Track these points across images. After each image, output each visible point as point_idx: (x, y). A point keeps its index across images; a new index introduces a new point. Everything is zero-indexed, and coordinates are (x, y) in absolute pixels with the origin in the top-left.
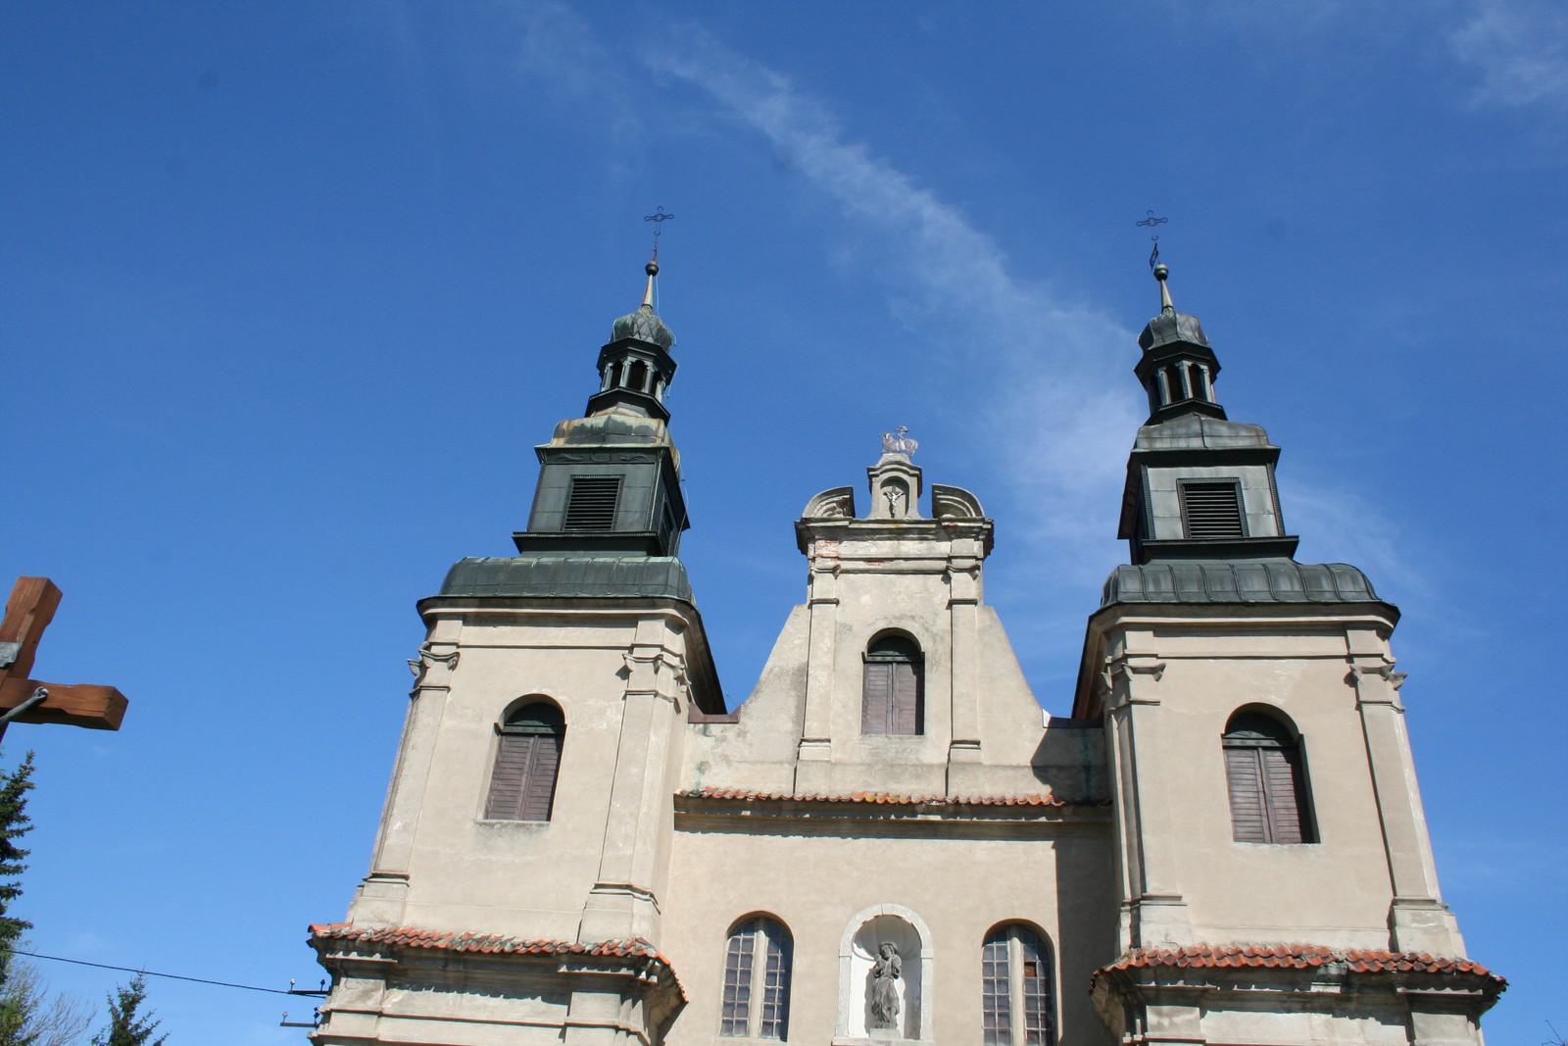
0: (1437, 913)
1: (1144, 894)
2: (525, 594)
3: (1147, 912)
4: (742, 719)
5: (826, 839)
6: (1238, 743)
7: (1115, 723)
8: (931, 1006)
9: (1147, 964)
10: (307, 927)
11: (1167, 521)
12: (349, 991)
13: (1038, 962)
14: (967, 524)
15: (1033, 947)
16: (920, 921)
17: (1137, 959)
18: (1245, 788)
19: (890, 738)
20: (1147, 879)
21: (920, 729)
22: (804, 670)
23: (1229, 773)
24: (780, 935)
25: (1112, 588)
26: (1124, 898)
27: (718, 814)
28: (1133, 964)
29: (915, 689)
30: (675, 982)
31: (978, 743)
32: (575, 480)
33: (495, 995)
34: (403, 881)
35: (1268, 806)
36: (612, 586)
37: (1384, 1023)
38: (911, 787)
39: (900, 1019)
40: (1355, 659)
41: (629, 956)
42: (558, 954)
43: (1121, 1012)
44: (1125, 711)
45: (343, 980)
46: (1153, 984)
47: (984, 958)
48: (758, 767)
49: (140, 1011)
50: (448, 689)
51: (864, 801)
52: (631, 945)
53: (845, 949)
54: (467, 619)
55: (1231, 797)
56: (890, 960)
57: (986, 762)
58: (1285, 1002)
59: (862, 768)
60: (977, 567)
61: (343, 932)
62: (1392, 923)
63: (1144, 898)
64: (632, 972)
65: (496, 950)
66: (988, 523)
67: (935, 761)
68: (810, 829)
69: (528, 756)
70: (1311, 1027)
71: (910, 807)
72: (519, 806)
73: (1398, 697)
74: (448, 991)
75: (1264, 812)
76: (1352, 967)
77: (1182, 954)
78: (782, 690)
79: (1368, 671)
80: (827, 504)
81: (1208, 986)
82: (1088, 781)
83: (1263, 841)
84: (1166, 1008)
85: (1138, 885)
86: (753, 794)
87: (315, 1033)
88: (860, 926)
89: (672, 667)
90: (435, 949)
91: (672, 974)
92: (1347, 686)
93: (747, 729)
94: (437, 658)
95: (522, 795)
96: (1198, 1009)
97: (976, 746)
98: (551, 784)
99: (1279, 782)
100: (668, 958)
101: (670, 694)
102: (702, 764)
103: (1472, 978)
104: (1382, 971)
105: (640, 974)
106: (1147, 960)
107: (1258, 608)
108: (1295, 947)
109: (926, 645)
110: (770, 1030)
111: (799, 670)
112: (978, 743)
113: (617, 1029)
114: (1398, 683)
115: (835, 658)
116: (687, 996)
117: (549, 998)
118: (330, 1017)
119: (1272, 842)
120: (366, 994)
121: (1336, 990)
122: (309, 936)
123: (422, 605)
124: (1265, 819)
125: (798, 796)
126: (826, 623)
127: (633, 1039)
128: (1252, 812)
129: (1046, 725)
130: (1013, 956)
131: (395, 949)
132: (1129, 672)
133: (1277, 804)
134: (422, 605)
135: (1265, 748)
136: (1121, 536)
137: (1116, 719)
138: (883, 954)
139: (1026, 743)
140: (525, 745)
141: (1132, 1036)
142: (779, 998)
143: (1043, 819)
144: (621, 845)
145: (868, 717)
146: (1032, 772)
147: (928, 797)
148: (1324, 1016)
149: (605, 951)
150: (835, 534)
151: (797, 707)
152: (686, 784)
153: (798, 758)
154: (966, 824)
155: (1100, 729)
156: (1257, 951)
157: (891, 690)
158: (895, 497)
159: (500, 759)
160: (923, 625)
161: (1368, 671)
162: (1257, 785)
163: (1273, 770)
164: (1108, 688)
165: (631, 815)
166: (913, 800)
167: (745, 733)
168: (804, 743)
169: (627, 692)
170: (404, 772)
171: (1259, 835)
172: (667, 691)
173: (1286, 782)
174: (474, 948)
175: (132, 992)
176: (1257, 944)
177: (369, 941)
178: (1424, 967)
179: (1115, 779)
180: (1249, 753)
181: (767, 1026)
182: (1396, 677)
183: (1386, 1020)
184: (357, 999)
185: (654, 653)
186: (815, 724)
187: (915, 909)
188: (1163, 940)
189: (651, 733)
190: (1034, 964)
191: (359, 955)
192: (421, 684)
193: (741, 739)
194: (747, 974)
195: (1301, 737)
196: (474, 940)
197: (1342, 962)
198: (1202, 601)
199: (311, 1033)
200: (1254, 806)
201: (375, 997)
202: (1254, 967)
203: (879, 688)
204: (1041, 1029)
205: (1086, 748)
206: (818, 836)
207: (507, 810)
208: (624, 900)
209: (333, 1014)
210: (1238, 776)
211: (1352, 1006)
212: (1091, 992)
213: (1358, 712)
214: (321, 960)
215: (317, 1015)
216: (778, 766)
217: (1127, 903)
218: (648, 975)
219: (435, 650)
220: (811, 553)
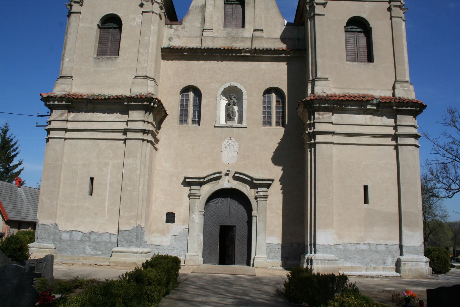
0: (409, 85)
1: (316, 77)
3: (317, 83)
4: (184, 23)
5: (212, 62)
6: (349, 30)
7: (309, 22)
8: (246, 114)
9: (316, 98)
10: (40, 94)
12: (56, 114)
13: (280, 101)
15: (279, 96)
17: (313, 97)
18: (351, 45)
19: (233, 29)
20: (317, 72)
21: (243, 26)
22: (204, 6)
23: (346, 40)
24: (198, 93)
26: (309, 79)
27: (176, 54)
28: (312, 98)
29: (242, 13)
30: (163, 107)
33: (104, 113)
34: (71, 78)
35: (358, 51)
37: (388, 118)
38: (241, 45)
39: (236, 118)
41: (147, 98)
42: (124, 98)
43: (307, 115)
44: (313, 18)
45: (54, 111)
46: (318, 105)
47: (263, 99)
48: (189, 39)
49: (8, 134)
50: (80, 13)
51: (224, 49)
52: (148, 95)
53: (218, 97)
55: (346, 47)
56: (233, 100)
57: (265, 37)
58: (358, 111)
61: (52, 95)
62: (394, 88)
63: (316, 78)
64: (148, 103)
65: (103, 98)
67: (248, 36)
68: (207, 59)
69: (110, 35)
70: (366, 119)
71: (240, 51)
72: (108, 52)
73: (404, 16)
74: (89, 113)
75: (356, 53)
76: (381, 101)
77: (327, 96)
78: (197, 13)
79: (395, 6)
81: (335, 106)
83: (355, 61)
84: (321, 113)
85: (314, 75)
86: (188, 47)
87: (47, 128)
88: (223, 89)
90: (82, 99)
91: (162, 104)
92: (388, 11)
93: (185, 26)
95: (109, 48)
96: (331, 113)
98: (119, 44)
99: (362, 43)
100: (159, 98)
101: (158, 12)
104: (390, 102)
105: (151, 104)
106: (316, 97)
108: (363, 95)
110: (195, 123)
111: (202, 6)
113: (144, 121)
114: (405, 11)
115: (214, 2)
116: (168, 112)
117: (122, 113)
118: (51, 123)
119: (358, 62)
120: (62, 115)
121: (375, 108)
122: (41, 97)
124: (356, 55)
125: (203, 48)
127: (150, 125)
129: (285, 25)
130: (272, 98)
131: (70, 100)
132: (315, 4)
133: (361, 50)
135: (358, 32)
137: (310, 21)
138: (231, 98)
139: (279, 31)
140: (109, 32)
141: (310, 121)
142: (197, 113)
143: (283, 55)
145: (226, 22)
146: (280, 40)
147: (246, 48)
148: (370, 116)
149: (139, 97)
152: (165, 44)
153: (202, 35)
154: (258, 57)
157: (233, 13)
159: (101, 37)
161: (395, 6)
164: (307, 10)
165: (146, 53)
166: (241, 49)
168: (204, 31)
169: (143, 11)
170: (68, 42)
171: (354, 60)
172: (157, 11)
173: (364, 43)
174: (95, 98)
175: (5, 128)
176: (351, 94)
177: (61, 97)
178: (403, 101)
179: (308, 41)
180: (353, 33)
181: (194, 122)
182: (404, 9)
183: (388, 117)
184: (59, 116)
186: (208, 24)
187: (241, 84)
188: (322, 91)
189: (152, 26)
190: (279, 101)
191: (58, 102)
192: (71, 11)
193: (183, 30)
194: (187, 105)
195: (371, 28)
196: (95, 95)
197: (378, 99)
199: (45, 128)
200: (353, 50)
201: (65, 115)
202: (350, 100)
203: (230, 12)
204: (280, 121)
206: (209, 61)
207: (104, 54)
208: (145, 81)
209: (52, 121)
210: (349, 41)
211: (379, 113)
212: (297, 109)
213: (390, 20)
214: (46, 105)
215: (47, 123)
216: (196, 38)
217: (311, 80)
218: (154, 104)
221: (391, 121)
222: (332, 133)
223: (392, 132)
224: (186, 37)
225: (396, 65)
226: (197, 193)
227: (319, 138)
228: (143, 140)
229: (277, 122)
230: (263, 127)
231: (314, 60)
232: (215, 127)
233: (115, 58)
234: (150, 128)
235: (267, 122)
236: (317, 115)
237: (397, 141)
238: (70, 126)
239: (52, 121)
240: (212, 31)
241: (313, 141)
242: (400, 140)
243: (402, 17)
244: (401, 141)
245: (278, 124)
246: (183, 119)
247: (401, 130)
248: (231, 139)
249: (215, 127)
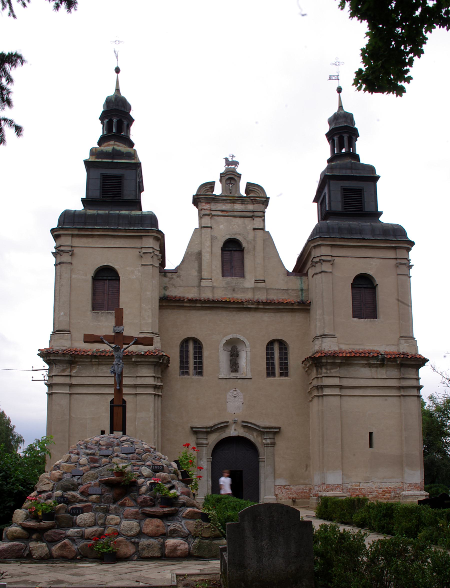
14: (260, 199)
16: (246, 340)
19: (233, 279)
31: (264, 281)
32: (103, 176)
38: (242, 295)
80: (206, 188)
82: (302, 295)
97: (263, 282)
102: (165, 287)
107: (368, 241)
109: (244, 245)
120: (64, 370)
136: (315, 201)
144: (147, 319)
155: (307, 277)
185: (151, 251)
186: (206, 273)
194: (187, 357)
205: (302, 283)
226: (205, 441)
239: (53, 377)
240: (211, 280)
243: (407, 275)
246: (184, 369)
248: (236, 390)
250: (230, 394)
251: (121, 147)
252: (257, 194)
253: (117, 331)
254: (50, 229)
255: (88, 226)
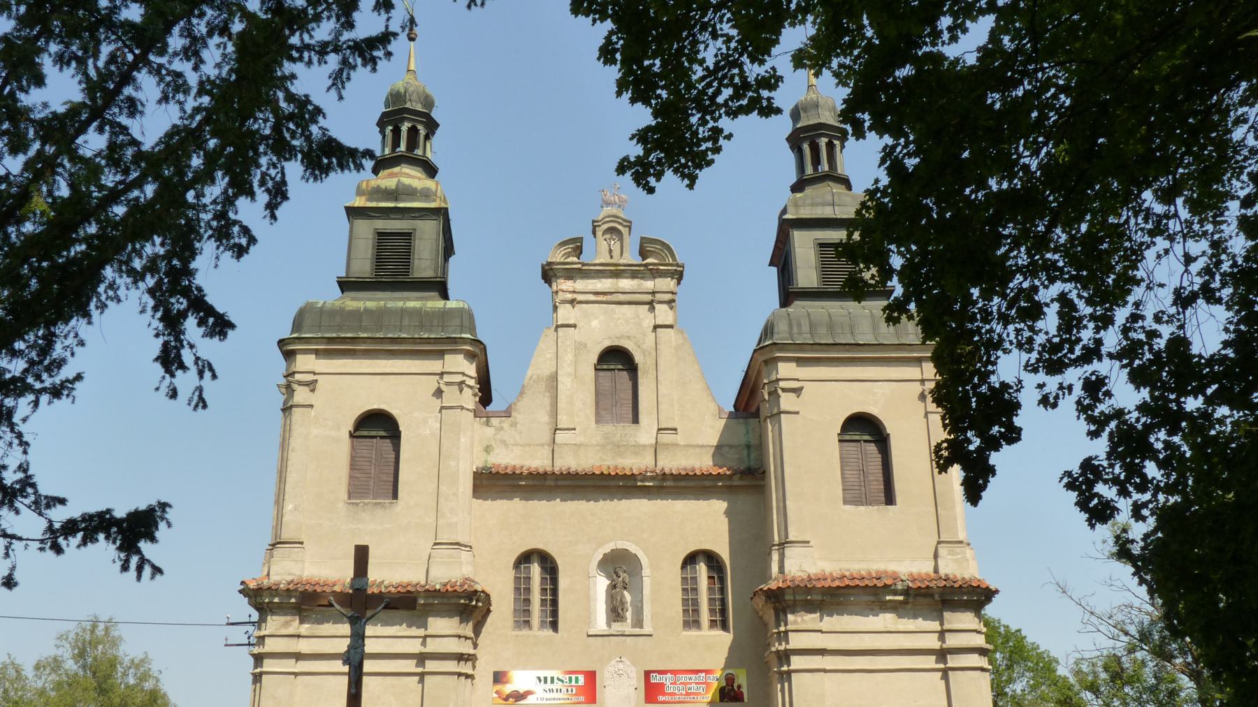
2: (362, 335)
3: (789, 552)
4: (513, 414)
11: (807, 274)
12: (274, 623)
18: (852, 468)
20: (789, 530)
21: (636, 420)
23: (841, 458)
24: (550, 568)
25: (768, 330)
34: (300, 546)
36: (422, 327)
38: (635, 461)
40: (926, 383)
43: (772, 612)
48: (527, 449)
50: (311, 406)
54: (317, 353)
55: (843, 474)
57: (682, 443)
59: (597, 448)
60: (673, 301)
62: (936, 556)
66: (680, 266)
67: (648, 442)
75: (863, 484)
76: (911, 585)
82: (749, 455)
89: (471, 387)
94: (300, 383)
99: (873, 464)
102: (487, 447)
103: (979, 590)
106: (789, 584)
107: (866, 347)
108: (877, 572)
109: (638, 358)
112: (676, 430)
113: (459, 637)
120: (287, 624)
121: (901, 598)
123: (281, 343)
124: (863, 488)
125: (557, 470)
126: (568, 343)
128: (855, 484)
130: (700, 573)
132: (780, 391)
134: (281, 343)
136: (771, 264)
138: (616, 573)
140: (371, 444)
144: (449, 516)
150: (571, 274)
151: (551, 404)
153: (554, 442)
155: (757, 420)
156: (855, 575)
158: (612, 242)
160: (636, 343)
162: (859, 466)
163: (869, 456)
165: (454, 494)
167: (516, 424)
168: (557, 432)
171: (859, 499)
173: (877, 463)
185: (459, 378)
187: (637, 544)
190: (713, 577)
193: (513, 428)
198: (829, 342)
205: (748, 432)
211: (909, 606)
219: (298, 377)
220: (554, 287)
221: (935, 626)
222: (822, 652)
223: (936, 645)
224: (521, 445)
225: (939, 509)
227: (797, 662)
228: (460, 674)
229: (711, 621)
230: (685, 633)
231: (781, 505)
232: (589, 636)
233: (391, 503)
234: (466, 648)
235: (692, 621)
236: (790, 617)
237: (945, 662)
238: (304, 646)
241: (782, 629)
242: (951, 659)
244: (953, 661)
245: (713, 624)
246: (522, 618)
247: (952, 641)
249: (589, 636)
250: (611, 669)
251: (413, 177)
252: (661, 257)
253: (356, 587)
254: (277, 340)
255: (347, 333)
